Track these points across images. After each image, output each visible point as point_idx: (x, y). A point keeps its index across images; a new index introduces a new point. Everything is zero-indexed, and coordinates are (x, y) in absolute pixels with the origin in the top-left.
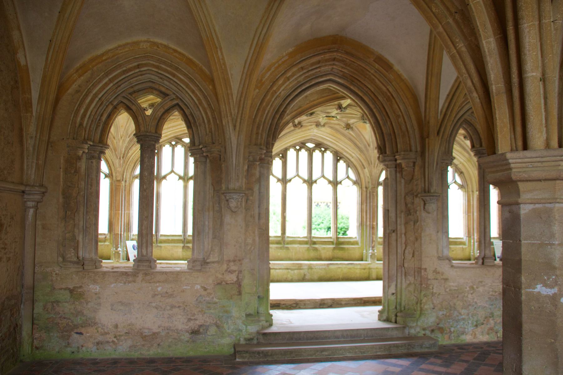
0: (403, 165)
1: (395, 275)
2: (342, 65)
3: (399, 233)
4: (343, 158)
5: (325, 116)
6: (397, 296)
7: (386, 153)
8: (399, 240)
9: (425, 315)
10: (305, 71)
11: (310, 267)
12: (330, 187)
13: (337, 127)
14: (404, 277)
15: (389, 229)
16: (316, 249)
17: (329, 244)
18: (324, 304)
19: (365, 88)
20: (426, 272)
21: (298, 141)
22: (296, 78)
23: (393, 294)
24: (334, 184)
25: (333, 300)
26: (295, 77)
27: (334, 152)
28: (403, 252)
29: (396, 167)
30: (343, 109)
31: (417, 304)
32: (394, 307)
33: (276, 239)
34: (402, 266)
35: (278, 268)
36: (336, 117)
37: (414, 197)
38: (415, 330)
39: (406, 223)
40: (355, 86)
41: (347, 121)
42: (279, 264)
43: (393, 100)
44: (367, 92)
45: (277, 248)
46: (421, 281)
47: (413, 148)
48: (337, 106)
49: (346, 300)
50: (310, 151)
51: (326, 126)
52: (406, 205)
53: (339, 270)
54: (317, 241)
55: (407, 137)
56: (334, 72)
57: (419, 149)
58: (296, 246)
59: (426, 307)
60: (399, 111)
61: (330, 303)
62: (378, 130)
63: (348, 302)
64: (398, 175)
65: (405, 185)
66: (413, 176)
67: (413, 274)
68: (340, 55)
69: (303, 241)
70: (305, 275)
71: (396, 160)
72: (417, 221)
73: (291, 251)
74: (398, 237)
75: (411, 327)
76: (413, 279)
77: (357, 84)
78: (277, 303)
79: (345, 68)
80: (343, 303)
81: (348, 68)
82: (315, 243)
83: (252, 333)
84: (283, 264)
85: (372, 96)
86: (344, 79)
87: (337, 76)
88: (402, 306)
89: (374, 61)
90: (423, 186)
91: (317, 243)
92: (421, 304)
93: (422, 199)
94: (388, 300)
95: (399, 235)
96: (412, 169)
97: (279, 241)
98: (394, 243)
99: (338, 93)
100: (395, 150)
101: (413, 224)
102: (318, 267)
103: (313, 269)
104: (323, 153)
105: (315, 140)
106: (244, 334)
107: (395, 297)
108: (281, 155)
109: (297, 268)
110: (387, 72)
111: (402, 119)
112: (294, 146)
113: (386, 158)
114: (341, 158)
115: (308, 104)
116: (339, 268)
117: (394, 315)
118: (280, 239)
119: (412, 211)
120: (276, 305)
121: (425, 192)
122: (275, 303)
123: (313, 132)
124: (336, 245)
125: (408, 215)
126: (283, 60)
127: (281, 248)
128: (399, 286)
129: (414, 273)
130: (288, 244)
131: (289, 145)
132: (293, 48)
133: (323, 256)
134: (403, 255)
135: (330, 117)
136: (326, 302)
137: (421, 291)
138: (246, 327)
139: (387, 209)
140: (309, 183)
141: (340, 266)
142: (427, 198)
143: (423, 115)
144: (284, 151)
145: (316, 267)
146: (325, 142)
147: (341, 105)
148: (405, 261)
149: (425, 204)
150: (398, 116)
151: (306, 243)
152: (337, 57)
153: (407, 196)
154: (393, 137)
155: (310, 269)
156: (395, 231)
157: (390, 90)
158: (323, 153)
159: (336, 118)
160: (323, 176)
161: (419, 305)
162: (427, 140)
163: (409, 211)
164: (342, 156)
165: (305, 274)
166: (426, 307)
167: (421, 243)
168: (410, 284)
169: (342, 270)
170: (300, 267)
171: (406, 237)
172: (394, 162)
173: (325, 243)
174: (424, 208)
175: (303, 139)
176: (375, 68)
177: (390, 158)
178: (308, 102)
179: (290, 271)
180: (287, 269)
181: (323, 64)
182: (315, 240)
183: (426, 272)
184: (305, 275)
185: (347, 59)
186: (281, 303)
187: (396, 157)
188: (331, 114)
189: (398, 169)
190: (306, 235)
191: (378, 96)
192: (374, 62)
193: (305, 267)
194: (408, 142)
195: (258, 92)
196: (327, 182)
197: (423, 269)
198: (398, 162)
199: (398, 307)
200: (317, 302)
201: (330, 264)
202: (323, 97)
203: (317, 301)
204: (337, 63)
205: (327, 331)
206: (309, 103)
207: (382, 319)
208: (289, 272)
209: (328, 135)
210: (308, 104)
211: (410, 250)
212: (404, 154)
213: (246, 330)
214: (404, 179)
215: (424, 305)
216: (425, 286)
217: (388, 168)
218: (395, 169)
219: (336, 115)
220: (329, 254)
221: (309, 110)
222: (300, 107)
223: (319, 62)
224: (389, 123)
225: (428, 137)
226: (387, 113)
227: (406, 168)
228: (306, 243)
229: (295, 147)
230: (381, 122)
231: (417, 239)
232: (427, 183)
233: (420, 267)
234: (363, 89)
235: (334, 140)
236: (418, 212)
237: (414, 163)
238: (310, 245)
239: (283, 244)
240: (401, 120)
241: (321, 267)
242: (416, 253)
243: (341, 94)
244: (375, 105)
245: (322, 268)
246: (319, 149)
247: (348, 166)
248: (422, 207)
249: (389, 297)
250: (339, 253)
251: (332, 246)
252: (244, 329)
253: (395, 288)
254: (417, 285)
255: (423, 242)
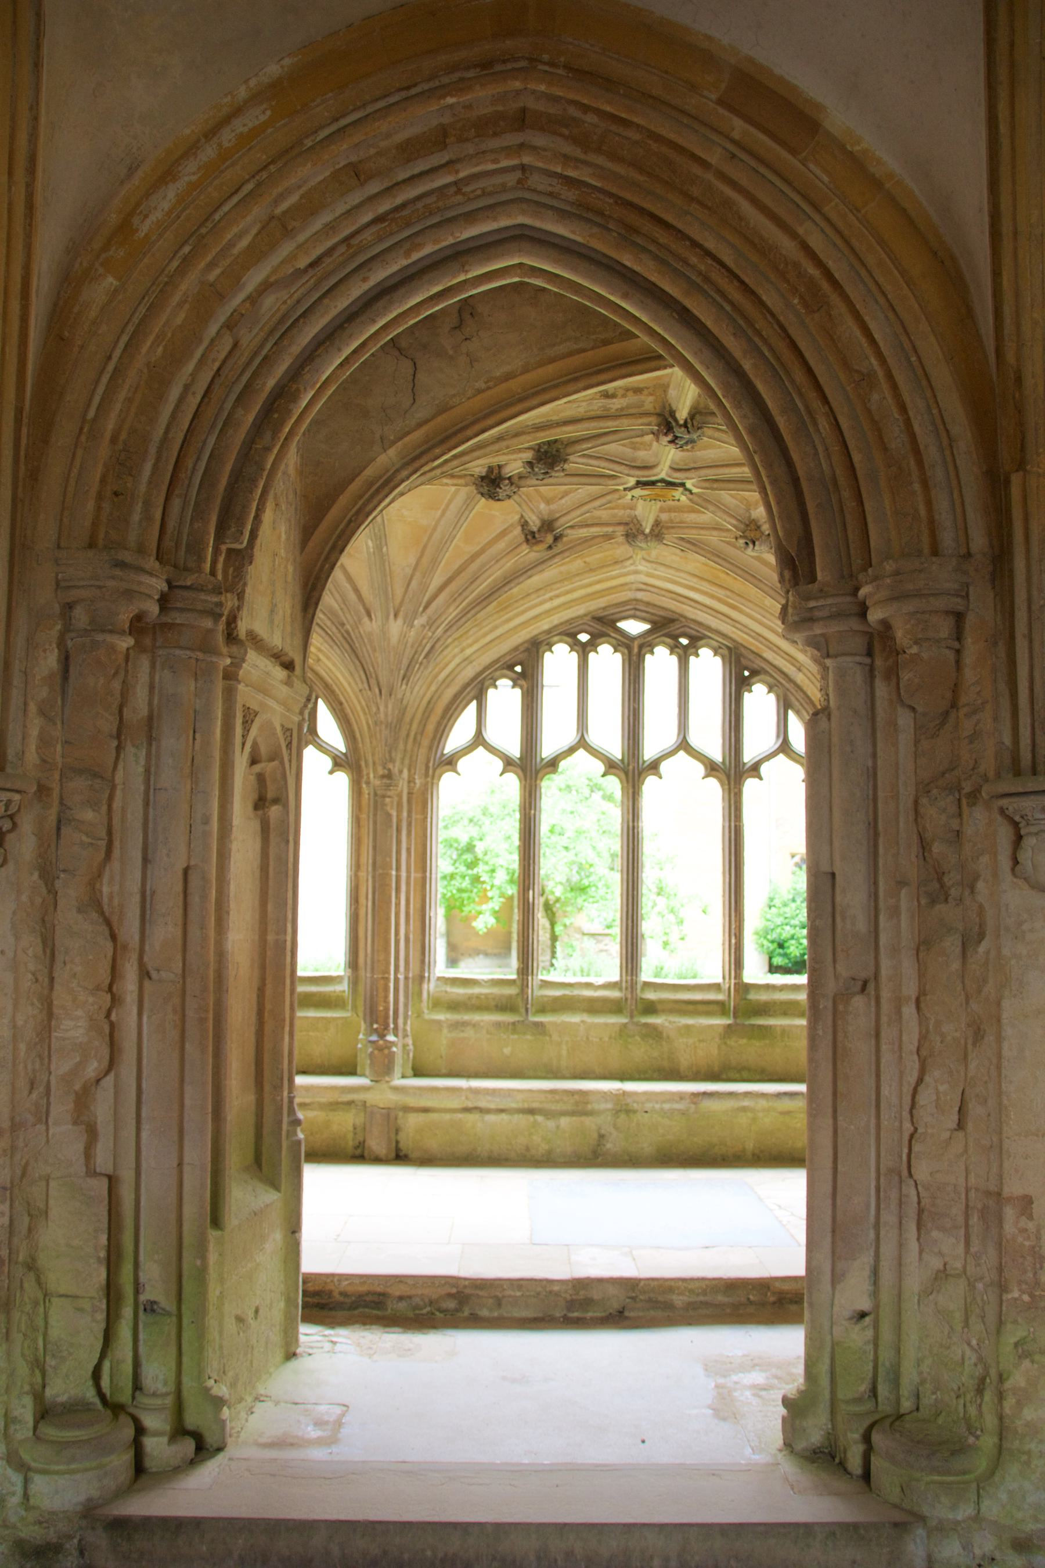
0: (901, 634)
1: (872, 1219)
2: (568, 149)
3: (886, 994)
4: (766, 672)
5: (632, 482)
6: (876, 1327)
7: (813, 579)
8: (888, 1033)
9: (1028, 1463)
10: (374, 187)
11: (623, 1105)
12: (714, 789)
13: (713, 539)
14: (912, 1227)
15: (836, 977)
16: (654, 1034)
17: (708, 1014)
18: (587, 1303)
19: (694, 260)
20: (1031, 1217)
21: (580, 610)
22: (326, 225)
23: (863, 1315)
24: (728, 777)
25: (630, 1285)
26: (325, 218)
27: (726, 652)
28: (907, 1100)
29: (870, 653)
30: (679, 432)
31: (980, 1391)
32: (864, 1387)
33: (496, 991)
34: (905, 1173)
35: (492, 1106)
36: (683, 485)
37: (964, 801)
38: (967, 1546)
39: (924, 945)
40: (644, 250)
41: (748, 510)
42: (494, 1092)
43: (834, 299)
44: (707, 279)
45: (498, 1025)
46: (1000, 1269)
47: (947, 539)
48: (653, 420)
49: (691, 1286)
50: (629, 648)
51: (669, 537)
52: (924, 845)
53: (743, 1120)
54: (661, 1001)
55: (917, 486)
56: (535, 191)
57: (979, 541)
58: (575, 1019)
59: (1029, 1414)
60: (868, 351)
61: (616, 1299)
62: (769, 466)
63: (701, 1298)
64: (881, 689)
65: (917, 742)
66: (956, 689)
67: (961, 1220)
68: (542, 88)
69: (605, 1000)
70: (601, 1136)
71: (862, 612)
72: (981, 936)
73: (556, 1037)
74: (884, 1019)
75: (941, 1529)
76: (961, 1249)
77: (654, 241)
78: (369, 1293)
79: (577, 160)
80: (678, 1300)
81: (600, 160)
82: (650, 1008)
83: (54, 1513)
84: (510, 1092)
85: (736, 295)
86: (588, 220)
87: (552, 208)
88: (905, 1391)
89: (720, 102)
90: (1007, 740)
91: (659, 1007)
92: (1001, 1396)
93: (1002, 811)
94: (834, 1345)
95: (885, 1006)
96: (951, 656)
97: (510, 997)
98: (860, 1049)
99: (630, 335)
100: (857, 562)
101: (958, 950)
102: (657, 1106)
103: (635, 1112)
104: (684, 656)
105: (648, 604)
106: (13, 1519)
107: (870, 1333)
108: (518, 669)
109: (569, 1107)
110: (793, 152)
111: (888, 393)
112: (569, 635)
113: (812, 604)
114: (754, 673)
115: (480, 391)
116: (744, 1109)
117: (857, 1436)
118: (513, 991)
119: (951, 879)
120: (369, 1298)
121: (1017, 773)
122: (363, 1289)
123: (636, 572)
124: (735, 1017)
125: (933, 902)
126: (242, 125)
127: (514, 1027)
128: (887, 1276)
129: (967, 1217)
130: (542, 1010)
131: (545, 625)
132: (287, 62)
133: (684, 1060)
134: (906, 1115)
135: (653, 483)
136: (596, 1295)
137: (1000, 1323)
138: (26, 1481)
139: (826, 868)
140: (626, 774)
141: (746, 1103)
142: (1027, 804)
143: (990, 345)
144: (527, 650)
145: (648, 1106)
146: (690, 612)
147: (672, 413)
148: (917, 1148)
149: (1018, 839)
150: (866, 380)
151: (615, 1007)
152: (531, 104)
153: (924, 801)
154: (846, 494)
155: (623, 1116)
156: (871, 987)
157: (816, 242)
158: (684, 656)
159: (681, 489)
160: (684, 745)
161: (988, 1396)
162: (1016, 479)
163: (940, 876)
164: (759, 663)
165: (603, 1132)
166: (1029, 1414)
167: (1000, 1056)
168: (943, 1275)
169: (754, 1119)
170: (581, 1105)
171: (922, 1019)
172: (855, 624)
173: (691, 1007)
174: (1016, 862)
175: (602, 602)
176: (733, 141)
177: (829, 601)
178: (481, 384)
179: (540, 1118)
180: (532, 1112)
181: (470, 149)
182: (651, 995)
183: (1031, 1217)
184: (601, 1136)
185: (586, 109)
186: (389, 1290)
187: (863, 592)
188: (655, 471)
189: (879, 662)
190: (615, 977)
191: (760, 291)
192: (721, 110)
193: (603, 1106)
194: (923, 512)
195: (116, 290)
196: (700, 769)
197: (1010, 1199)
198: (874, 616)
199: (883, 1390)
200: (557, 1294)
201: (705, 1094)
202: (552, 360)
203: (556, 1288)
204: (540, 140)
205: (455, 1525)
206: (489, 388)
207: (800, 1445)
208: (535, 1124)
209: (693, 582)
210: (480, 391)
211: (942, 1088)
212: (897, 573)
213: (26, 1496)
214: (913, 709)
215: (1019, 1405)
216: (1026, 1298)
217: (828, 656)
218: (868, 661)
219: (677, 477)
220: (709, 1052)
221: (490, 421)
222: (443, 410)
223: (439, 139)
224: (824, 423)
225: (1021, 465)
226: (810, 371)
227: (915, 650)
228: (615, 1007)
229: (573, 636)
230: (781, 422)
231: (978, 1035)
232: (1025, 720)
233: (993, 1188)
234: (685, 262)
235: (720, 600)
236: (980, 885)
237: (959, 617)
238: (632, 1017)
239: (523, 1010)
240: (881, 397)
241: (667, 1106)
242: (975, 1109)
243: (645, 338)
244: (750, 340)
245: (672, 1111)
246: (668, 640)
247: (785, 705)
248: (1005, 863)
249: (837, 1331)
250: (750, 1050)
251: (720, 1021)
252: (14, 1494)
253: (867, 1286)
254: (980, 1286)
255: (1008, 1050)
